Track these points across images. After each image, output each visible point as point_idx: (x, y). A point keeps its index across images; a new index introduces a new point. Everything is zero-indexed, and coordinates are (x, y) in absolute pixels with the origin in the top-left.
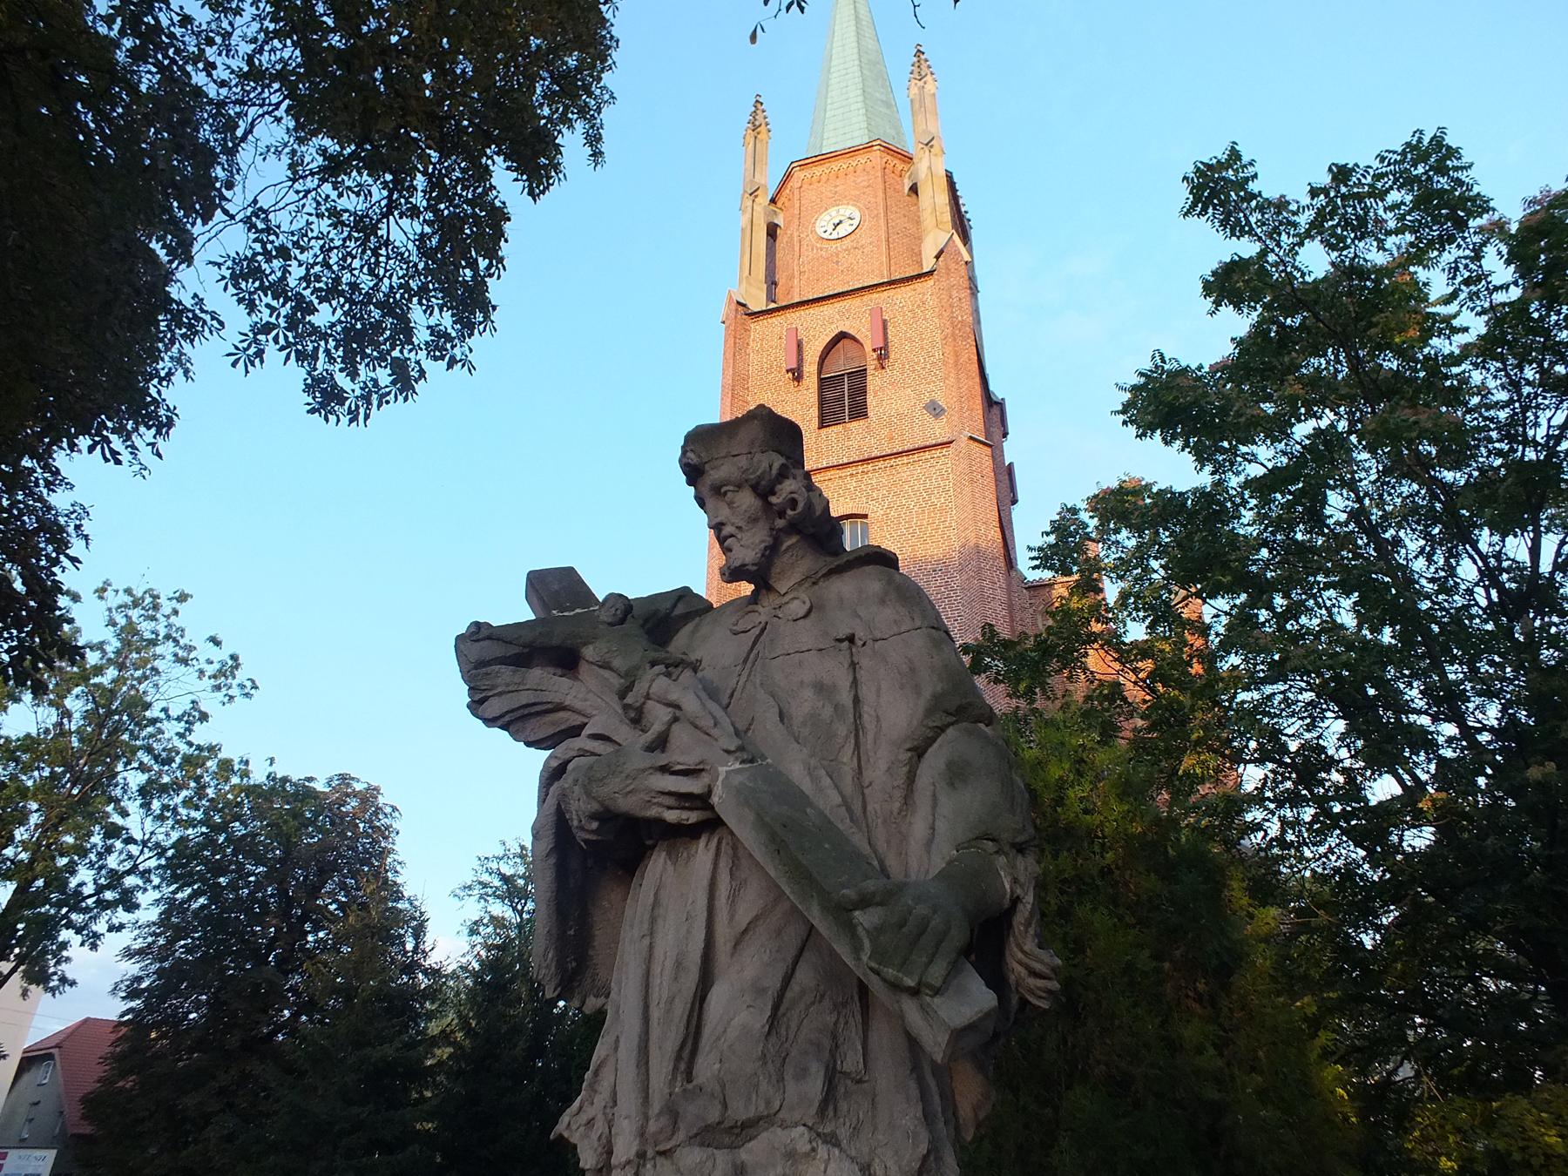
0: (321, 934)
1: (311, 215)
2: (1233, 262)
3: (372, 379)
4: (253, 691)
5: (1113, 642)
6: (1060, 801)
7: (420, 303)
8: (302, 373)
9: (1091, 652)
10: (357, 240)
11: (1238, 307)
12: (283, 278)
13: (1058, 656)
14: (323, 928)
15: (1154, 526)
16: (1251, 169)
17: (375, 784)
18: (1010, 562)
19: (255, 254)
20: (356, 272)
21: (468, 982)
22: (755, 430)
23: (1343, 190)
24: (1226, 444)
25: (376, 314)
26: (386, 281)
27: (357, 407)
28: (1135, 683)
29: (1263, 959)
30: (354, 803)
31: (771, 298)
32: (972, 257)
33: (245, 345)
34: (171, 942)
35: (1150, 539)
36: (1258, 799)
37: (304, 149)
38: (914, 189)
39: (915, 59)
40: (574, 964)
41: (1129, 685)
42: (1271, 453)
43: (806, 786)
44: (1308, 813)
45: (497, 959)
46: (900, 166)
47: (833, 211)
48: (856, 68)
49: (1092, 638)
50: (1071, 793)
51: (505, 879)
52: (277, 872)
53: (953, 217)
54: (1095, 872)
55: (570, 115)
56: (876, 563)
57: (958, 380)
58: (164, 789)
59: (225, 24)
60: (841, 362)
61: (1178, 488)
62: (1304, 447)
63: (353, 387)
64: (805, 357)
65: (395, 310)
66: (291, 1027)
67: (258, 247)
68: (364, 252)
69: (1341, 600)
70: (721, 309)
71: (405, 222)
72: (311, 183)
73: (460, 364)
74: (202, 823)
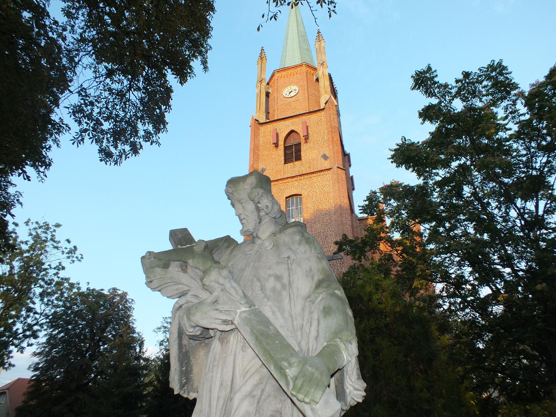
0: (106, 346)
1: (102, 90)
2: (429, 106)
4: (81, 259)
6: (370, 300)
7: (141, 122)
11: (431, 121)
16: (435, 73)
17: (125, 291)
19: (81, 104)
22: (252, 180)
23: (467, 81)
24: (427, 169)
28: (397, 255)
30: (118, 298)
31: (267, 118)
33: (77, 137)
34: (51, 350)
38: (317, 80)
39: (317, 35)
40: (185, 381)
42: (444, 173)
46: (312, 72)
49: (381, 239)
50: (374, 297)
52: (90, 324)
57: (333, 147)
58: (49, 294)
59: (72, 23)
60: (292, 141)
62: (455, 170)
64: (279, 139)
66: (94, 380)
68: (121, 103)
70: (249, 122)
71: (135, 93)
72: (102, 79)
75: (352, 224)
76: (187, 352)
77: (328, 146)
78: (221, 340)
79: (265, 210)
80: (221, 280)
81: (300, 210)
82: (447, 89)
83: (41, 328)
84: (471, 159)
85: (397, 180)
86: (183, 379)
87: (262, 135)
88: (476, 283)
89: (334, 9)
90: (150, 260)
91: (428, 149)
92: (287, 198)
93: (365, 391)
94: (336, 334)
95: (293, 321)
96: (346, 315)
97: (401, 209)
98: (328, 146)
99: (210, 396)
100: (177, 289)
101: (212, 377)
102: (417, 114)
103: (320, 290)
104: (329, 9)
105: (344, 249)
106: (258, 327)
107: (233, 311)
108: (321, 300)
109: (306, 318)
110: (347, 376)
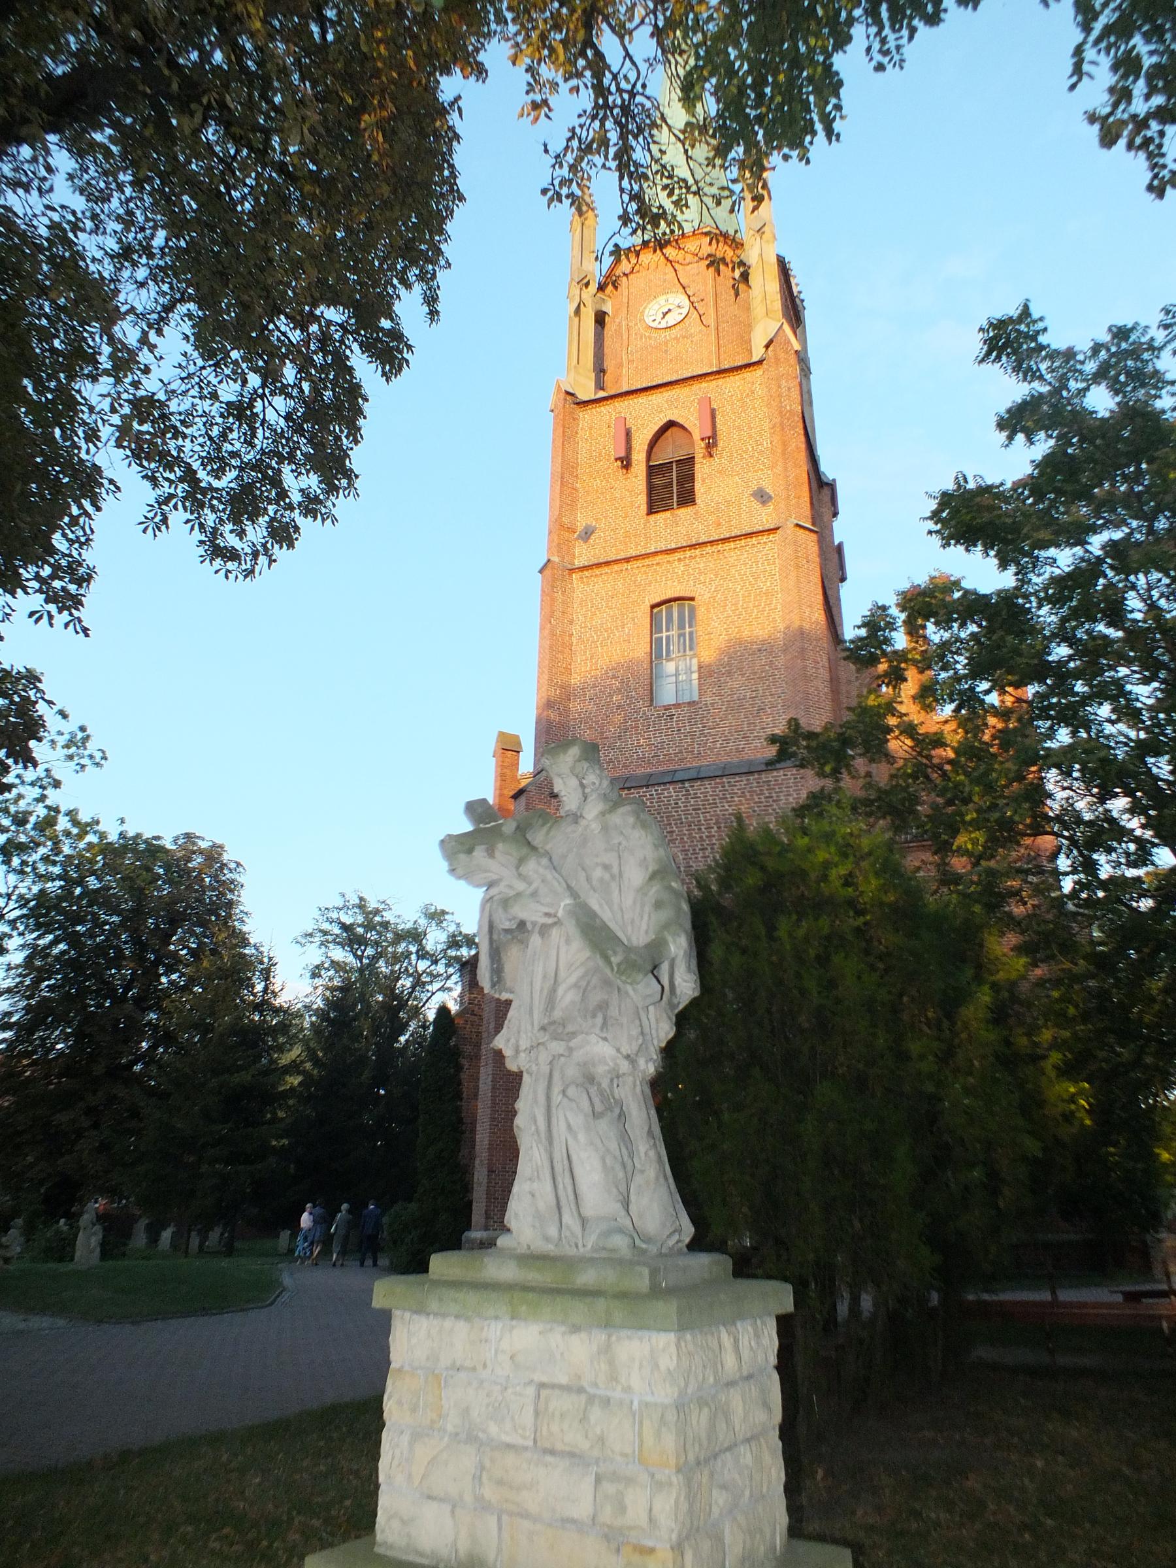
0: (174, 977)
1: (194, 397)
4: (103, 762)
6: (825, 878)
17: (218, 842)
31: (600, 386)
34: (37, 982)
47: (662, 299)
51: (345, 927)
52: (133, 920)
56: (802, 370)
57: (786, 469)
58: (22, 848)
60: (670, 448)
66: (148, 1057)
70: (549, 398)
74: (59, 877)
77: (772, 468)
80: (541, 870)
81: (691, 639)
83: (13, 930)
87: (583, 434)
88: (1148, 834)
92: (653, 607)
94: (666, 926)
96: (679, 909)
98: (772, 468)
105: (794, 755)
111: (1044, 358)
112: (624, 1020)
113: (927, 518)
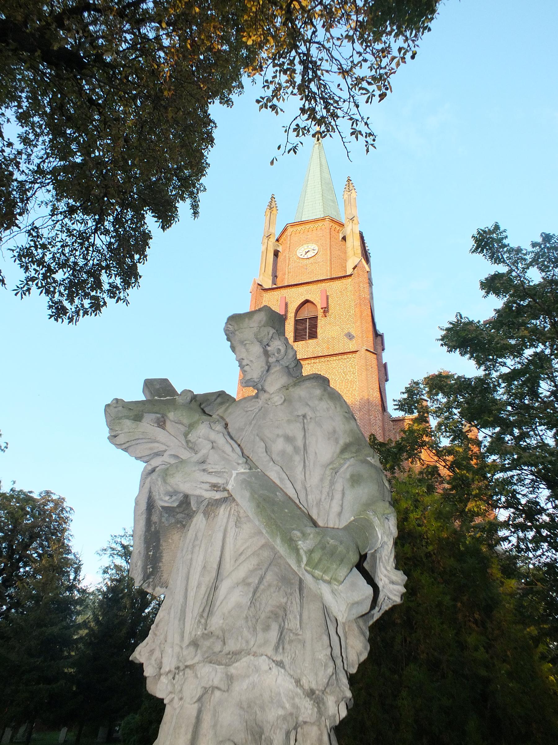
0: (27, 569)
1: (58, 231)
2: (495, 274)
3: (81, 304)
5: (434, 446)
7: (106, 273)
8: (48, 299)
9: (423, 450)
10: (79, 243)
11: (498, 294)
12: (43, 257)
13: (407, 451)
14: (29, 565)
15: (456, 394)
16: (504, 234)
17: (63, 496)
18: (384, 408)
19: (31, 247)
20: (77, 257)
21: (100, 597)
22: (262, 317)
23: (548, 245)
24: (491, 357)
25: (85, 276)
26: (91, 262)
27: (73, 316)
28: (444, 467)
29: (510, 605)
30: (51, 505)
31: (274, 283)
32: (370, 269)
33: (22, 286)
35: (453, 400)
36: (505, 525)
37: (59, 204)
38: (344, 238)
39: (347, 183)
40: (151, 570)
41: (441, 468)
42: (513, 362)
43: (277, 482)
44: (530, 534)
45: (115, 586)
46: (338, 228)
48: (320, 185)
49: (423, 444)
50: (411, 515)
51: (124, 547)
53: (362, 253)
54: (422, 555)
55: (185, 195)
59: (29, 150)
60: (306, 313)
61: (467, 376)
62: (529, 360)
63: (71, 307)
64: (289, 310)
65: (94, 273)
67: (32, 244)
68: (82, 249)
69: (548, 431)
70: (251, 286)
71: (102, 237)
72: (60, 217)
73: (122, 301)
75: (383, 425)
76: (157, 533)
78: (206, 514)
79: (276, 354)
82: (520, 255)
84: (552, 346)
85: (447, 369)
86: (148, 567)
89: (372, 142)
90: (116, 409)
91: (493, 331)
93: (406, 586)
94: (368, 505)
95: (307, 495)
97: (453, 407)
99: (187, 584)
100: (151, 449)
101: (191, 559)
102: (479, 285)
103: (346, 455)
104: (367, 142)
106: (261, 492)
107: (227, 473)
108: (348, 467)
109: (326, 490)
110: (381, 564)
111: (505, 252)
112: (308, 635)
113: (439, 340)
